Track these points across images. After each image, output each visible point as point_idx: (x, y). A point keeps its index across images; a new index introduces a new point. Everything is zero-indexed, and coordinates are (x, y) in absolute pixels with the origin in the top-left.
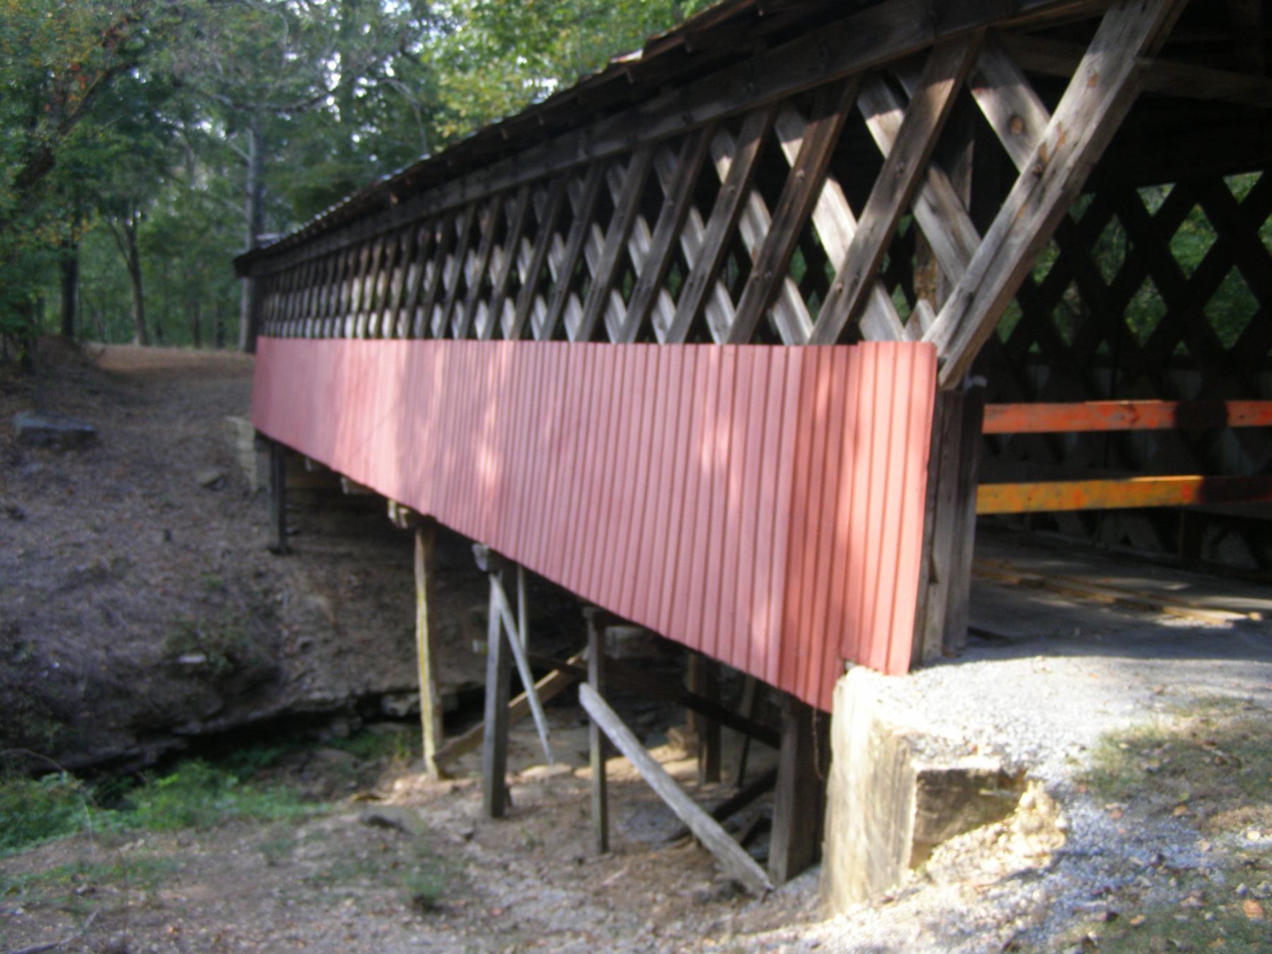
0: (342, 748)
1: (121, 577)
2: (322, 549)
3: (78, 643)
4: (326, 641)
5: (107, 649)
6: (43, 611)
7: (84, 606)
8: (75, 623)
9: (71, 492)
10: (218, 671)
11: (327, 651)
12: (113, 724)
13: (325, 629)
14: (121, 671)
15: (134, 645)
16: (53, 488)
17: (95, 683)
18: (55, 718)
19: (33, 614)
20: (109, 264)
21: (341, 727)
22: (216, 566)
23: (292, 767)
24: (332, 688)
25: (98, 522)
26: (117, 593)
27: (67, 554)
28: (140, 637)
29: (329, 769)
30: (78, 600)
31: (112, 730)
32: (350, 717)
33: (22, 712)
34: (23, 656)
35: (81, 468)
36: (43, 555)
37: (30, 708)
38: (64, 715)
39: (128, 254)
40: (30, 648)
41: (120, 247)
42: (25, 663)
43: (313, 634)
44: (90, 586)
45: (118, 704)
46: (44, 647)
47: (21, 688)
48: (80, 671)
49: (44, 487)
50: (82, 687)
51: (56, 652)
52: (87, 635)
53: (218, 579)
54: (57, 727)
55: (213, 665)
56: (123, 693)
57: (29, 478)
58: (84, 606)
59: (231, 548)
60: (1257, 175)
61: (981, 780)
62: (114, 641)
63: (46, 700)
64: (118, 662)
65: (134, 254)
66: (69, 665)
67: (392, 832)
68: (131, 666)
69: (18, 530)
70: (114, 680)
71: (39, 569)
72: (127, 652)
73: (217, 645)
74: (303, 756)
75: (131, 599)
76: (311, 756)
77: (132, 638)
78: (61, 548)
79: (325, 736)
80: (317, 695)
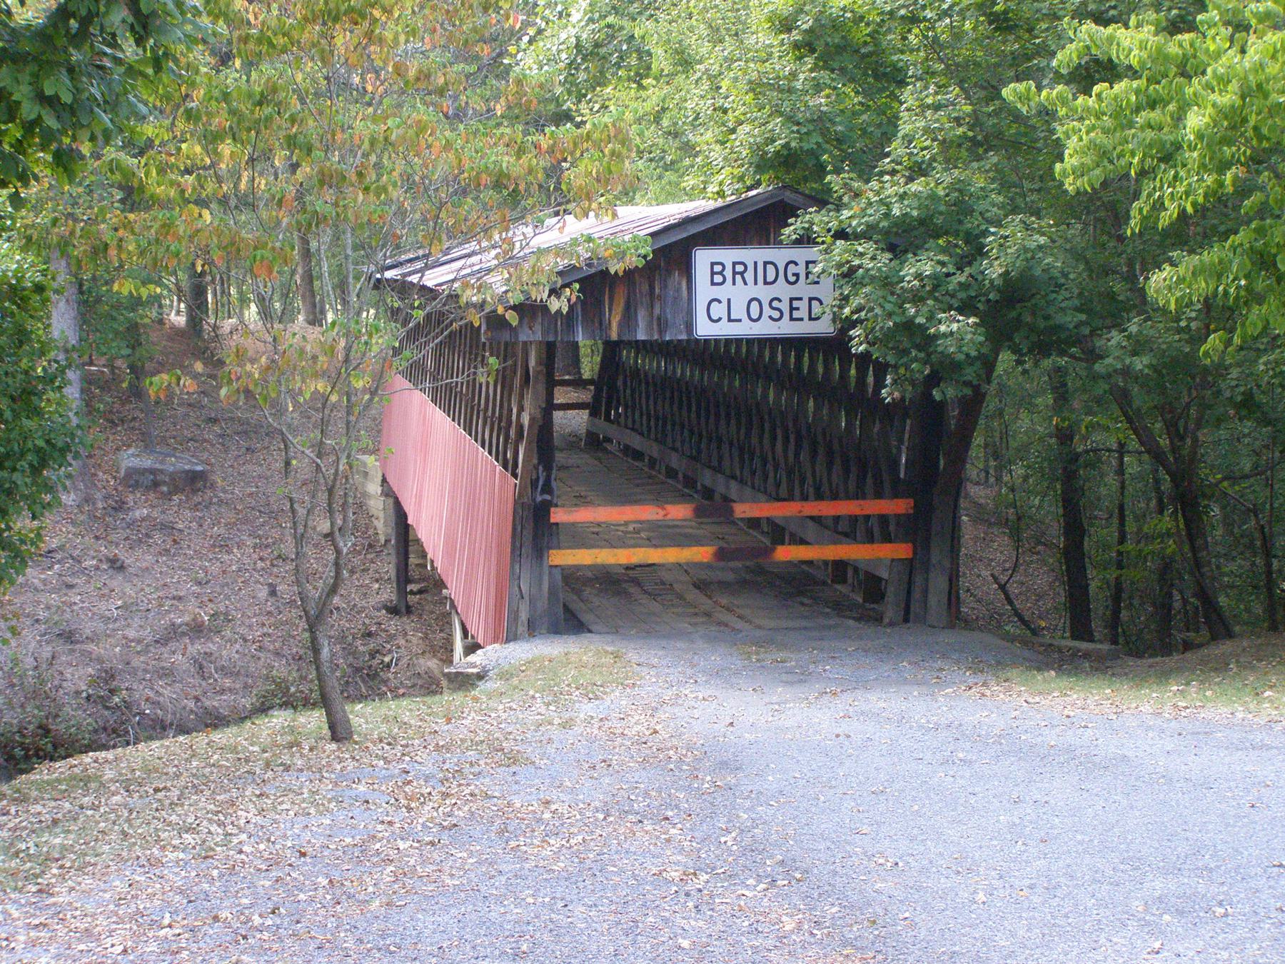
5: (197, 699)
16: (158, 537)
61: (468, 676)
69: (117, 581)
77: (222, 692)
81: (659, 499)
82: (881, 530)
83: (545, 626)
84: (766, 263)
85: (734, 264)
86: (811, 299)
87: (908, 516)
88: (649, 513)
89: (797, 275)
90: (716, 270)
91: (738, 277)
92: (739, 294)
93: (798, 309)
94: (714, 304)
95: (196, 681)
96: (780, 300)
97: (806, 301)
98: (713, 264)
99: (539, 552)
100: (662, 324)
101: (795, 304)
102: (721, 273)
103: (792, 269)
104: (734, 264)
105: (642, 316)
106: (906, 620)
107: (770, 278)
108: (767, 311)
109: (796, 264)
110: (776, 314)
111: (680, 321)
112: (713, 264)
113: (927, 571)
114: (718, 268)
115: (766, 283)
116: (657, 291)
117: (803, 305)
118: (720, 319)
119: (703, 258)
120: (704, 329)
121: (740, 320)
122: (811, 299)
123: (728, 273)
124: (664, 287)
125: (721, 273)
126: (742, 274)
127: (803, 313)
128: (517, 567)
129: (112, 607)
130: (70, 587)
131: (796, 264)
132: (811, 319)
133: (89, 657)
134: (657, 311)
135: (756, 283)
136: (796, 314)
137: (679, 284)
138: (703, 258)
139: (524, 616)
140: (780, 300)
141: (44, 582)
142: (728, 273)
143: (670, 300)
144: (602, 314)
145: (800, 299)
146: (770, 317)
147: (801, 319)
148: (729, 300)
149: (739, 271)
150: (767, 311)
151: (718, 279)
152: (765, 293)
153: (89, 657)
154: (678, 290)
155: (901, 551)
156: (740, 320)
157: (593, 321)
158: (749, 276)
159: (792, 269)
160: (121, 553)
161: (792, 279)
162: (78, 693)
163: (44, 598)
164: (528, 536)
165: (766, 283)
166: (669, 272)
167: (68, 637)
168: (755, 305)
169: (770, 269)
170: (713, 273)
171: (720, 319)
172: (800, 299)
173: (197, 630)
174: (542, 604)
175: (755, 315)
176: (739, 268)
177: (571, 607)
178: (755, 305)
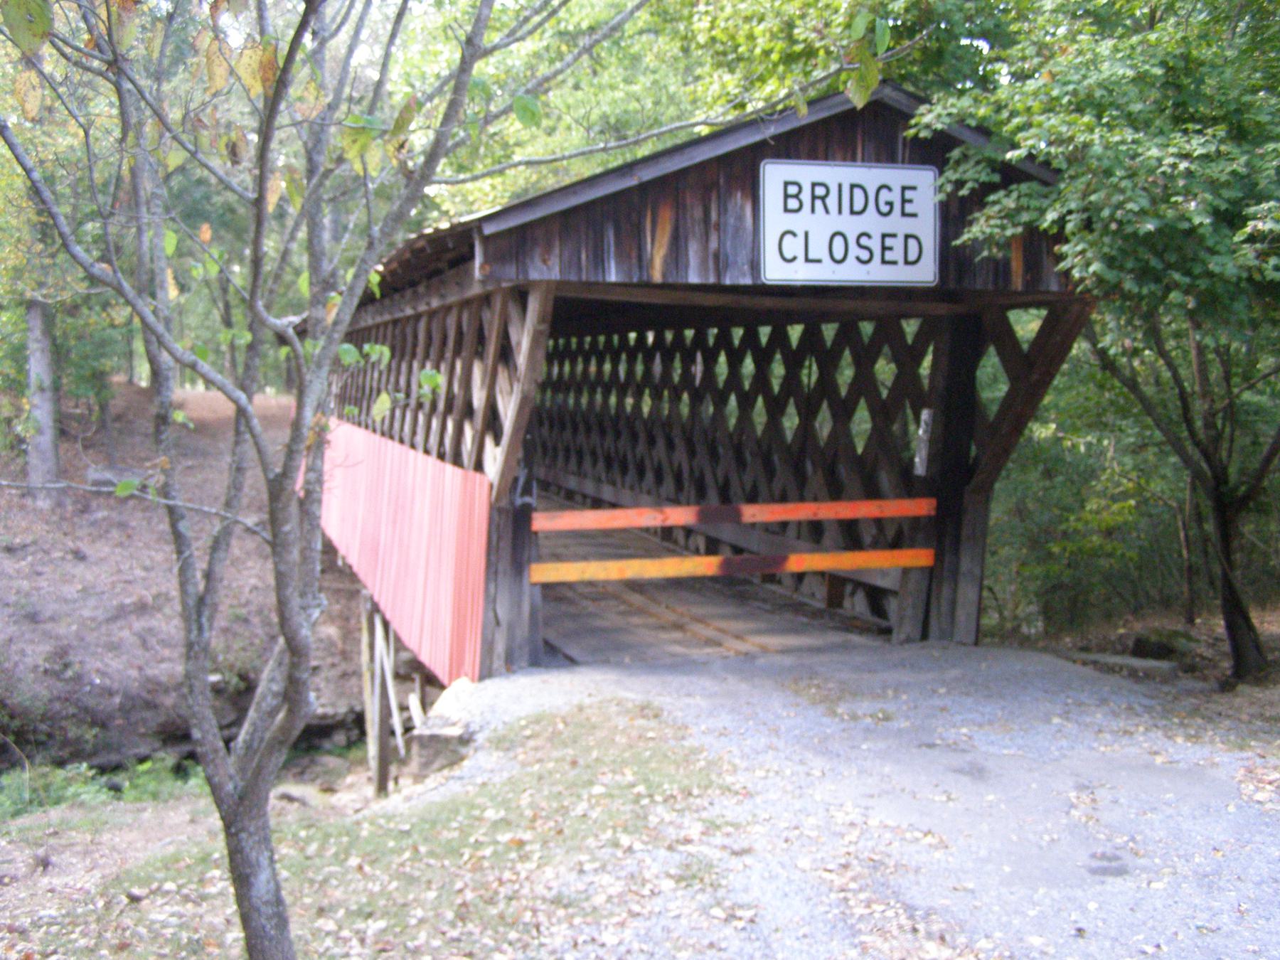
0: (340, 755)
1: (159, 609)
2: (341, 586)
3: (115, 664)
4: (333, 665)
5: (140, 669)
6: (91, 637)
7: (126, 634)
8: (114, 647)
9: (129, 537)
10: (231, 689)
11: (334, 673)
12: (142, 730)
13: (333, 655)
14: (150, 686)
15: (164, 666)
16: (115, 534)
17: (127, 696)
18: (93, 724)
19: (82, 639)
20: (207, 315)
21: (340, 738)
22: (243, 600)
23: (295, 770)
24: (333, 705)
25: (148, 563)
26: (154, 623)
27: (118, 590)
28: (170, 660)
29: (326, 773)
30: (121, 628)
31: (143, 735)
32: (349, 729)
33: (66, 718)
34: (69, 673)
35: (139, 515)
36: (98, 590)
37: (74, 715)
38: (102, 723)
39: (221, 305)
40: (77, 667)
41: (214, 301)
42: (71, 679)
43: (323, 659)
44: (133, 617)
45: (148, 714)
46: (88, 667)
47: (67, 700)
48: (116, 686)
49: (107, 531)
50: (117, 700)
51: (98, 671)
52: (125, 657)
53: (244, 611)
54: (95, 731)
55: (227, 683)
56: (151, 706)
57: (94, 524)
58: (126, 634)
59: (260, 584)
60: (829, 344)
61: (447, 740)
62: (147, 663)
63: (86, 710)
64: (149, 680)
65: (227, 306)
66: (108, 682)
67: (296, 805)
68: (159, 684)
69: (80, 570)
70: (145, 694)
71: (92, 602)
72: (157, 672)
73: (231, 667)
74: (306, 761)
75: (164, 628)
76: (313, 762)
77: (162, 660)
78: (113, 585)
79: (327, 744)
80: (320, 711)
81: (660, 501)
82: (895, 536)
83: (526, 657)
84: (852, 187)
85: (814, 185)
86: (907, 237)
87: (930, 518)
88: (646, 517)
89: (890, 204)
90: (790, 192)
91: (818, 203)
92: (819, 225)
93: (890, 249)
94: (788, 238)
95: (140, 652)
96: (869, 236)
97: (901, 239)
98: (786, 184)
99: (519, 567)
100: (720, 261)
101: (889, 242)
102: (796, 196)
103: (884, 195)
104: (814, 185)
105: (693, 251)
106: (976, 643)
107: (858, 206)
108: (854, 250)
109: (889, 189)
110: (865, 255)
111: (743, 257)
112: (786, 184)
113: (956, 582)
114: (792, 190)
115: (852, 212)
116: (714, 216)
117: (897, 244)
118: (794, 259)
119: (774, 175)
120: (775, 272)
121: (819, 261)
122: (907, 237)
123: (806, 196)
124: (722, 211)
125: (796, 196)
126: (823, 199)
127: (896, 255)
128: (492, 587)
129: (71, 591)
130: (39, 574)
131: (889, 189)
132: (907, 262)
133: (47, 635)
134: (713, 244)
135: (840, 212)
136: (889, 256)
137: (742, 208)
138: (774, 175)
139: (500, 648)
140: (869, 236)
141: (18, 571)
142: (806, 196)
143: (730, 230)
144: (640, 248)
145: (894, 236)
146: (858, 259)
147: (895, 263)
148: (806, 234)
149: (819, 197)
150: (854, 250)
151: (793, 204)
152: (853, 227)
153: (47, 635)
154: (740, 218)
155: (919, 557)
156: (819, 261)
157: (629, 257)
158: (832, 201)
159: (884, 195)
160: (85, 547)
161: (885, 209)
162: (36, 667)
163: (16, 584)
164: (506, 545)
165: (852, 212)
166: (730, 193)
167: (33, 618)
168: (838, 241)
169: (858, 194)
170: (786, 196)
171: (794, 259)
172: (894, 236)
173: (142, 608)
174: (523, 631)
175: (838, 254)
176: (820, 191)
177: (552, 634)
178: (838, 241)
